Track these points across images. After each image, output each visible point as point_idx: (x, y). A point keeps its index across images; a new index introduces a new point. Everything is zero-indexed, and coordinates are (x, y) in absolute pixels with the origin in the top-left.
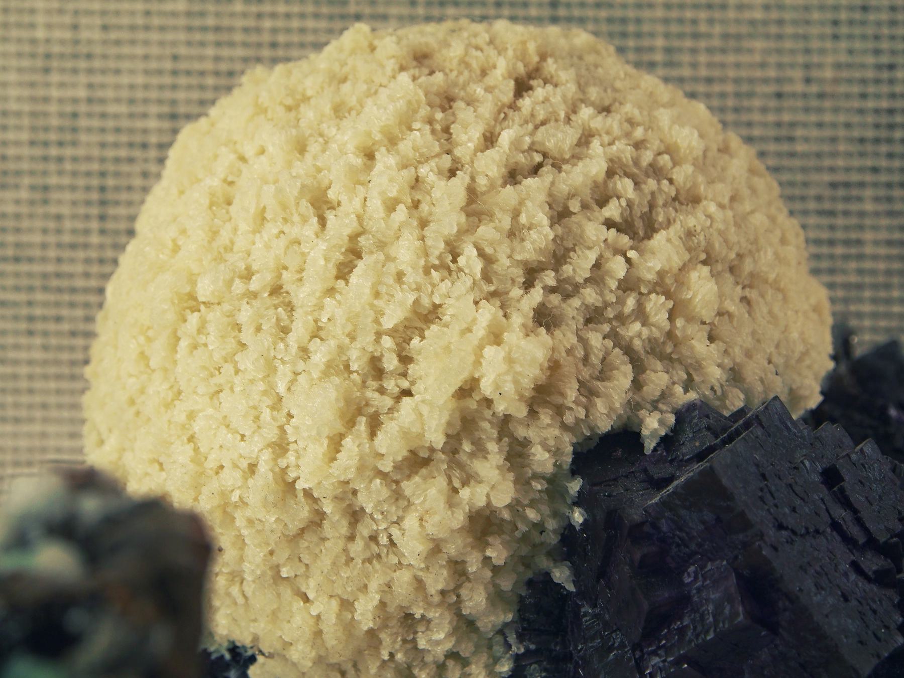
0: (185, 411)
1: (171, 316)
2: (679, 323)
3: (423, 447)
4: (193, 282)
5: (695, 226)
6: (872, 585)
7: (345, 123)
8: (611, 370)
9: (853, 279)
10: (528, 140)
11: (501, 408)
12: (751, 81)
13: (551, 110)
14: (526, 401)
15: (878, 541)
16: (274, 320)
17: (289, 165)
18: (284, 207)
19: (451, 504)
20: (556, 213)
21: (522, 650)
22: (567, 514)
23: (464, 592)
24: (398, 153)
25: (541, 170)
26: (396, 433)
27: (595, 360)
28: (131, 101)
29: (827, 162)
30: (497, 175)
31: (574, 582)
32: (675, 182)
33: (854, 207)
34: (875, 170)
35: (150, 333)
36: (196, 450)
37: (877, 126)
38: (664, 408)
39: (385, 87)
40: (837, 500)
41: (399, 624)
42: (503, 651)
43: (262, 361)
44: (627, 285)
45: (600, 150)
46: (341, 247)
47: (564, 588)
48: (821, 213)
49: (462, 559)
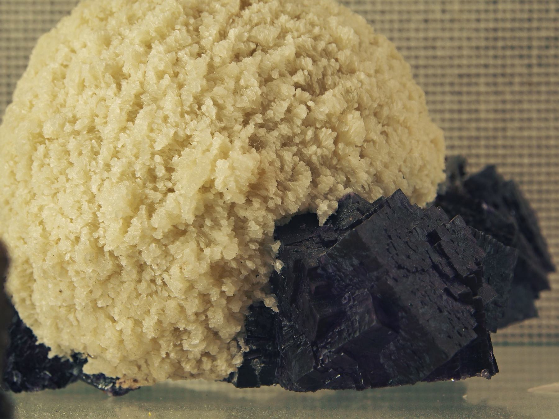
0: (37, 206)
1: (27, 147)
2: (341, 146)
3: (181, 223)
4: (41, 126)
5: (351, 87)
6: (458, 303)
7: (135, 27)
8: (298, 175)
9: (474, 133)
10: (246, 35)
11: (228, 198)
12: (409, 12)
13: (261, 17)
14: (244, 194)
15: (462, 276)
16: (90, 148)
17: (100, 53)
18: (96, 78)
19: (199, 258)
20: (263, 79)
21: (248, 350)
22: (272, 264)
23: (209, 313)
24: (166, 43)
25: (254, 53)
26: (164, 215)
27: (288, 168)
28: (26, 30)
29: (456, 62)
30: (227, 56)
31: (278, 306)
32: (339, 60)
33: (474, 89)
34: (486, 66)
35: (17, 159)
36: (44, 229)
37: (487, 39)
38: (331, 198)
39: (160, 4)
40: (436, 252)
41: (171, 335)
42: (237, 352)
43: (82, 173)
44: (308, 123)
45: (291, 40)
46: (130, 101)
47: (272, 310)
48: (453, 93)
49: (207, 293)
